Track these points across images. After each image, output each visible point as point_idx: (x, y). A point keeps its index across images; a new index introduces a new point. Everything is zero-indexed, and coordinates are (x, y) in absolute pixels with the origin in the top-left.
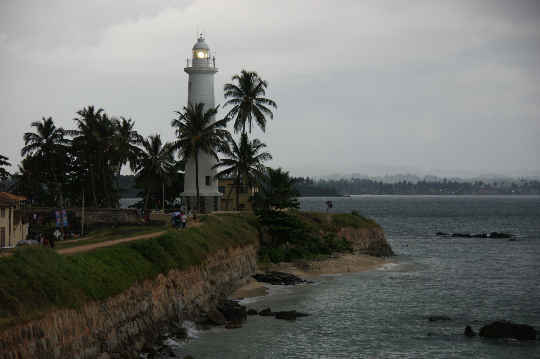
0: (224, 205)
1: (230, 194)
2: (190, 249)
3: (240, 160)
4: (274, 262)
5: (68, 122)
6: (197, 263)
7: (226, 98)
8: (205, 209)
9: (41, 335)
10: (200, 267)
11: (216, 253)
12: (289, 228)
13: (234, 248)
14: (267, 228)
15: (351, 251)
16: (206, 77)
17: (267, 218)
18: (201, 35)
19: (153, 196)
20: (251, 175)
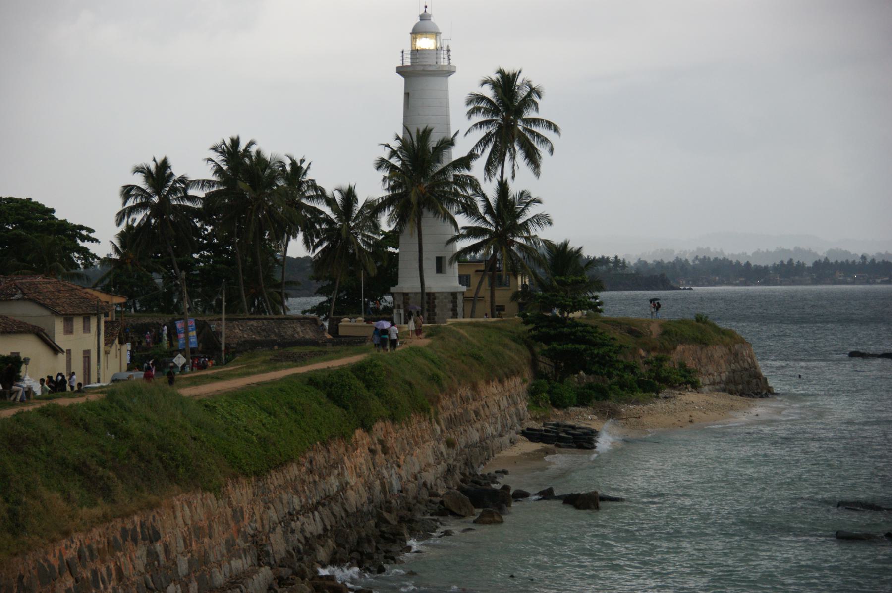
1: (478, 288)
3: (496, 228)
5: (196, 166)
6: (424, 410)
7: (469, 118)
8: (435, 314)
9: (155, 536)
10: (428, 417)
11: (456, 392)
12: (583, 347)
13: (487, 382)
15: (695, 386)
17: (544, 330)
18: (426, 7)
19: (345, 292)
20: (515, 254)
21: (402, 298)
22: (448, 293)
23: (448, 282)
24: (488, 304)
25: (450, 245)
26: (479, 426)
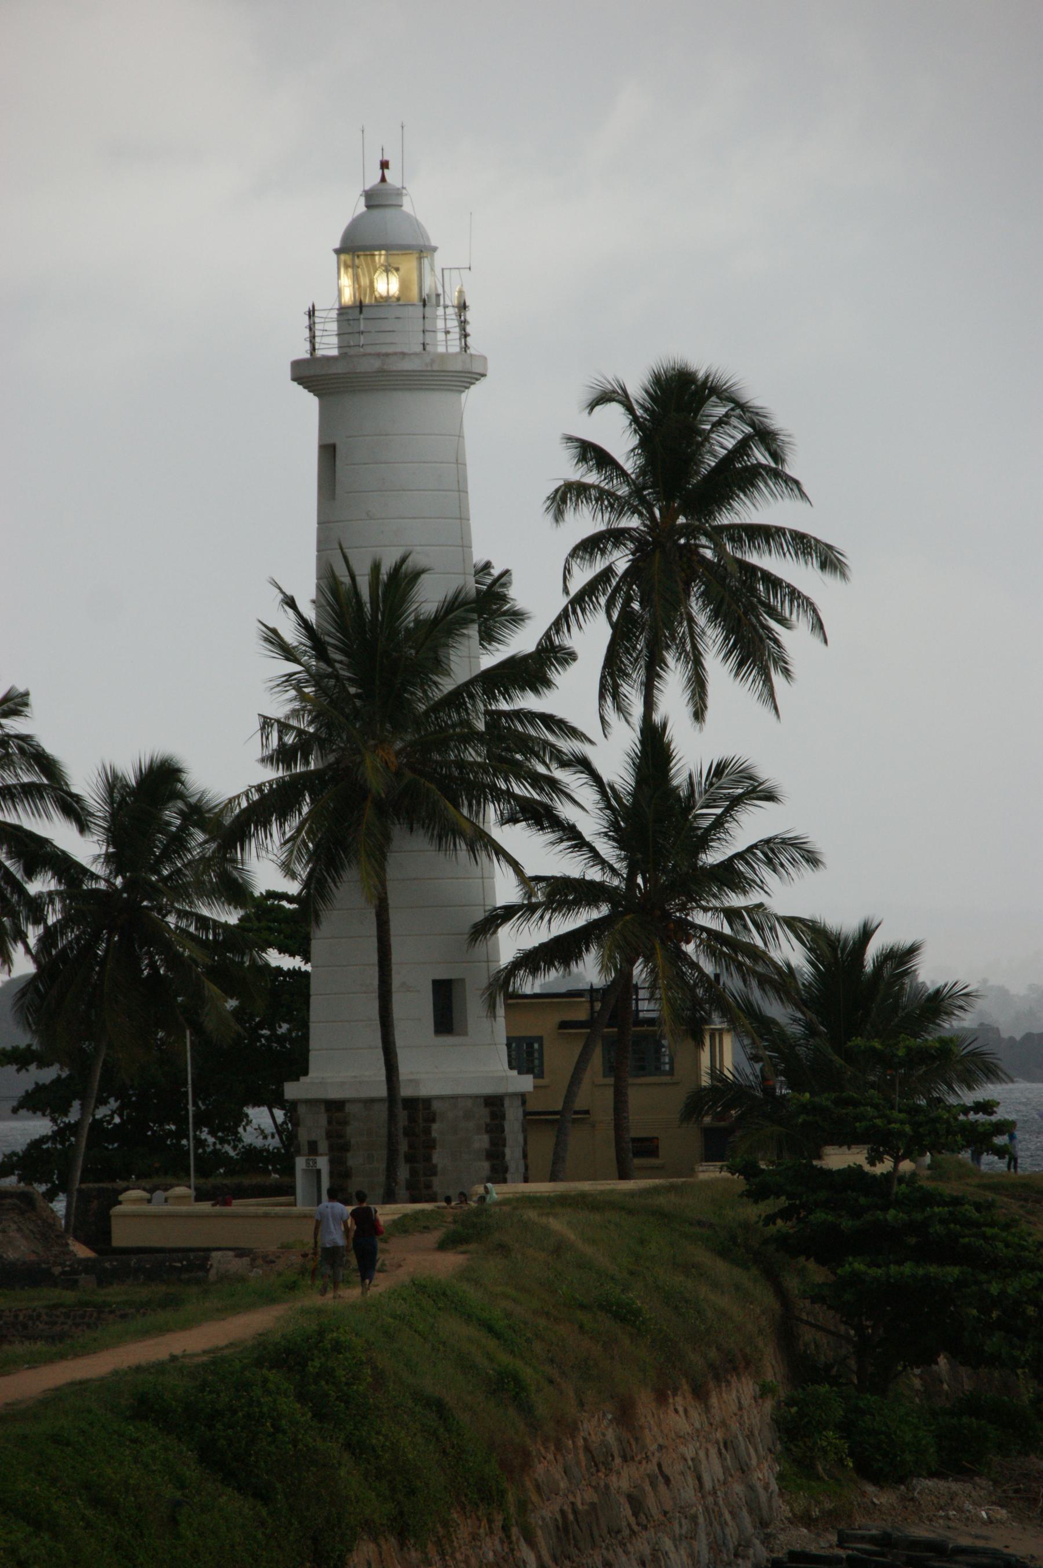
0: (543, 1144)
1: (575, 1080)
2: (439, 1407)
3: (630, 880)
4: (878, 1479)
6: (488, 1495)
7: (559, 515)
8: (433, 1171)
10: (499, 1519)
11: (573, 1430)
12: (955, 1271)
13: (661, 1398)
14: (818, 1274)
16: (421, 409)
17: (819, 1216)
18: (384, 165)
19: (113, 1104)
20: (695, 966)
21: (323, 1119)
22: (476, 1097)
23: (470, 1066)
24: (606, 1132)
25: (480, 948)
26: (647, 1551)
